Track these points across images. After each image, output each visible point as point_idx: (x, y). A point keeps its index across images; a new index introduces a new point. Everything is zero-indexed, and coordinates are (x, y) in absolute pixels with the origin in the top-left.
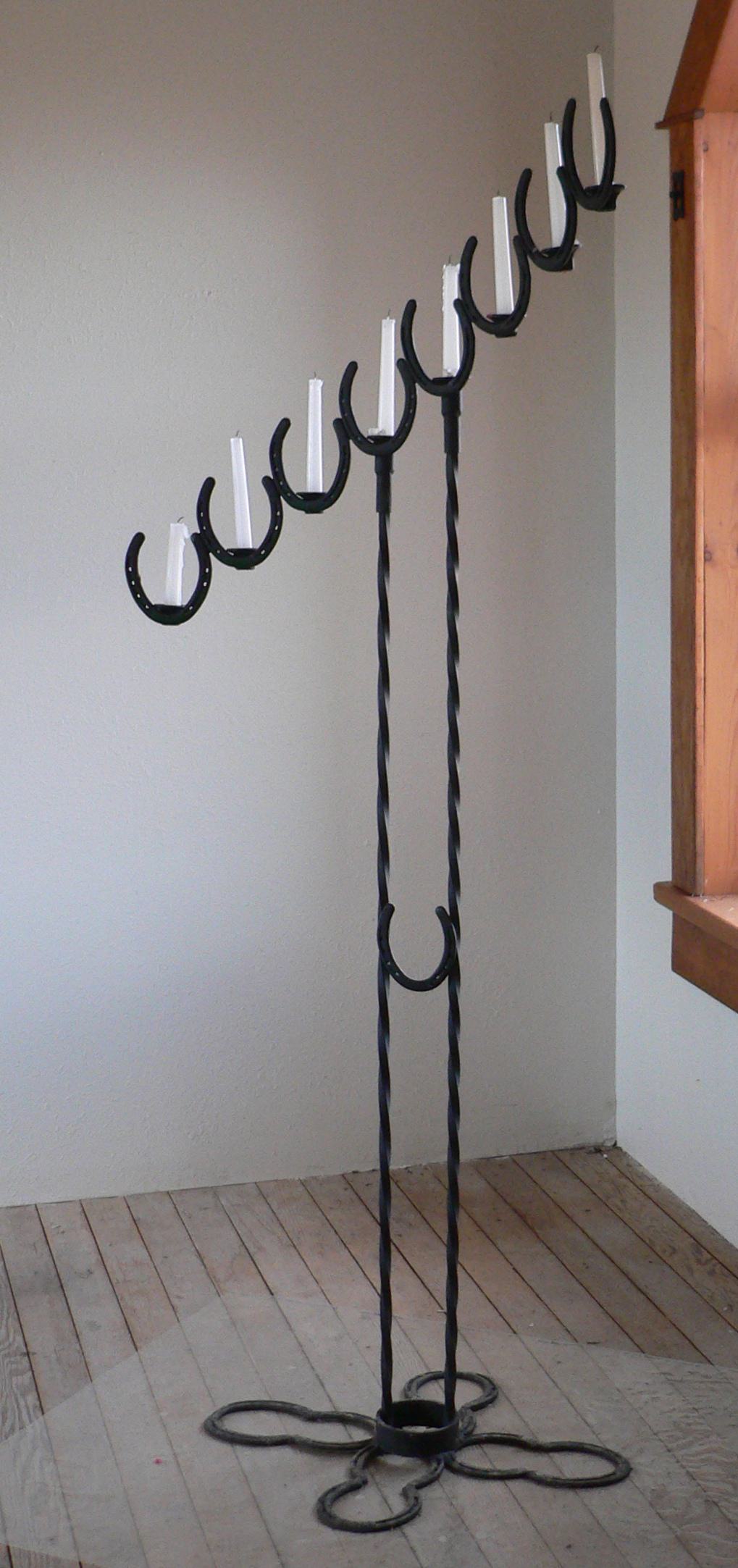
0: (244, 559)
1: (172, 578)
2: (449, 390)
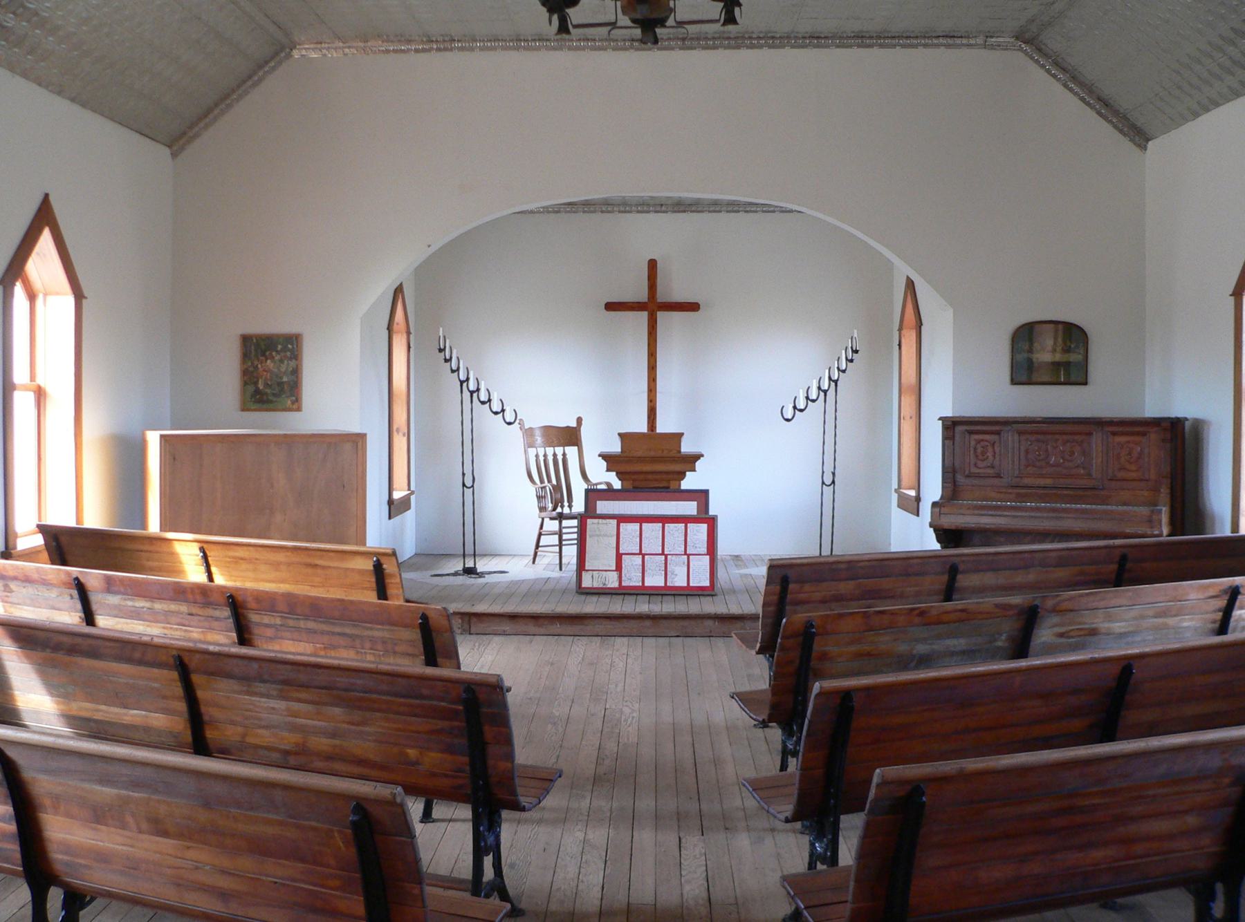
0: (801, 410)
1: (789, 413)
2: (836, 382)
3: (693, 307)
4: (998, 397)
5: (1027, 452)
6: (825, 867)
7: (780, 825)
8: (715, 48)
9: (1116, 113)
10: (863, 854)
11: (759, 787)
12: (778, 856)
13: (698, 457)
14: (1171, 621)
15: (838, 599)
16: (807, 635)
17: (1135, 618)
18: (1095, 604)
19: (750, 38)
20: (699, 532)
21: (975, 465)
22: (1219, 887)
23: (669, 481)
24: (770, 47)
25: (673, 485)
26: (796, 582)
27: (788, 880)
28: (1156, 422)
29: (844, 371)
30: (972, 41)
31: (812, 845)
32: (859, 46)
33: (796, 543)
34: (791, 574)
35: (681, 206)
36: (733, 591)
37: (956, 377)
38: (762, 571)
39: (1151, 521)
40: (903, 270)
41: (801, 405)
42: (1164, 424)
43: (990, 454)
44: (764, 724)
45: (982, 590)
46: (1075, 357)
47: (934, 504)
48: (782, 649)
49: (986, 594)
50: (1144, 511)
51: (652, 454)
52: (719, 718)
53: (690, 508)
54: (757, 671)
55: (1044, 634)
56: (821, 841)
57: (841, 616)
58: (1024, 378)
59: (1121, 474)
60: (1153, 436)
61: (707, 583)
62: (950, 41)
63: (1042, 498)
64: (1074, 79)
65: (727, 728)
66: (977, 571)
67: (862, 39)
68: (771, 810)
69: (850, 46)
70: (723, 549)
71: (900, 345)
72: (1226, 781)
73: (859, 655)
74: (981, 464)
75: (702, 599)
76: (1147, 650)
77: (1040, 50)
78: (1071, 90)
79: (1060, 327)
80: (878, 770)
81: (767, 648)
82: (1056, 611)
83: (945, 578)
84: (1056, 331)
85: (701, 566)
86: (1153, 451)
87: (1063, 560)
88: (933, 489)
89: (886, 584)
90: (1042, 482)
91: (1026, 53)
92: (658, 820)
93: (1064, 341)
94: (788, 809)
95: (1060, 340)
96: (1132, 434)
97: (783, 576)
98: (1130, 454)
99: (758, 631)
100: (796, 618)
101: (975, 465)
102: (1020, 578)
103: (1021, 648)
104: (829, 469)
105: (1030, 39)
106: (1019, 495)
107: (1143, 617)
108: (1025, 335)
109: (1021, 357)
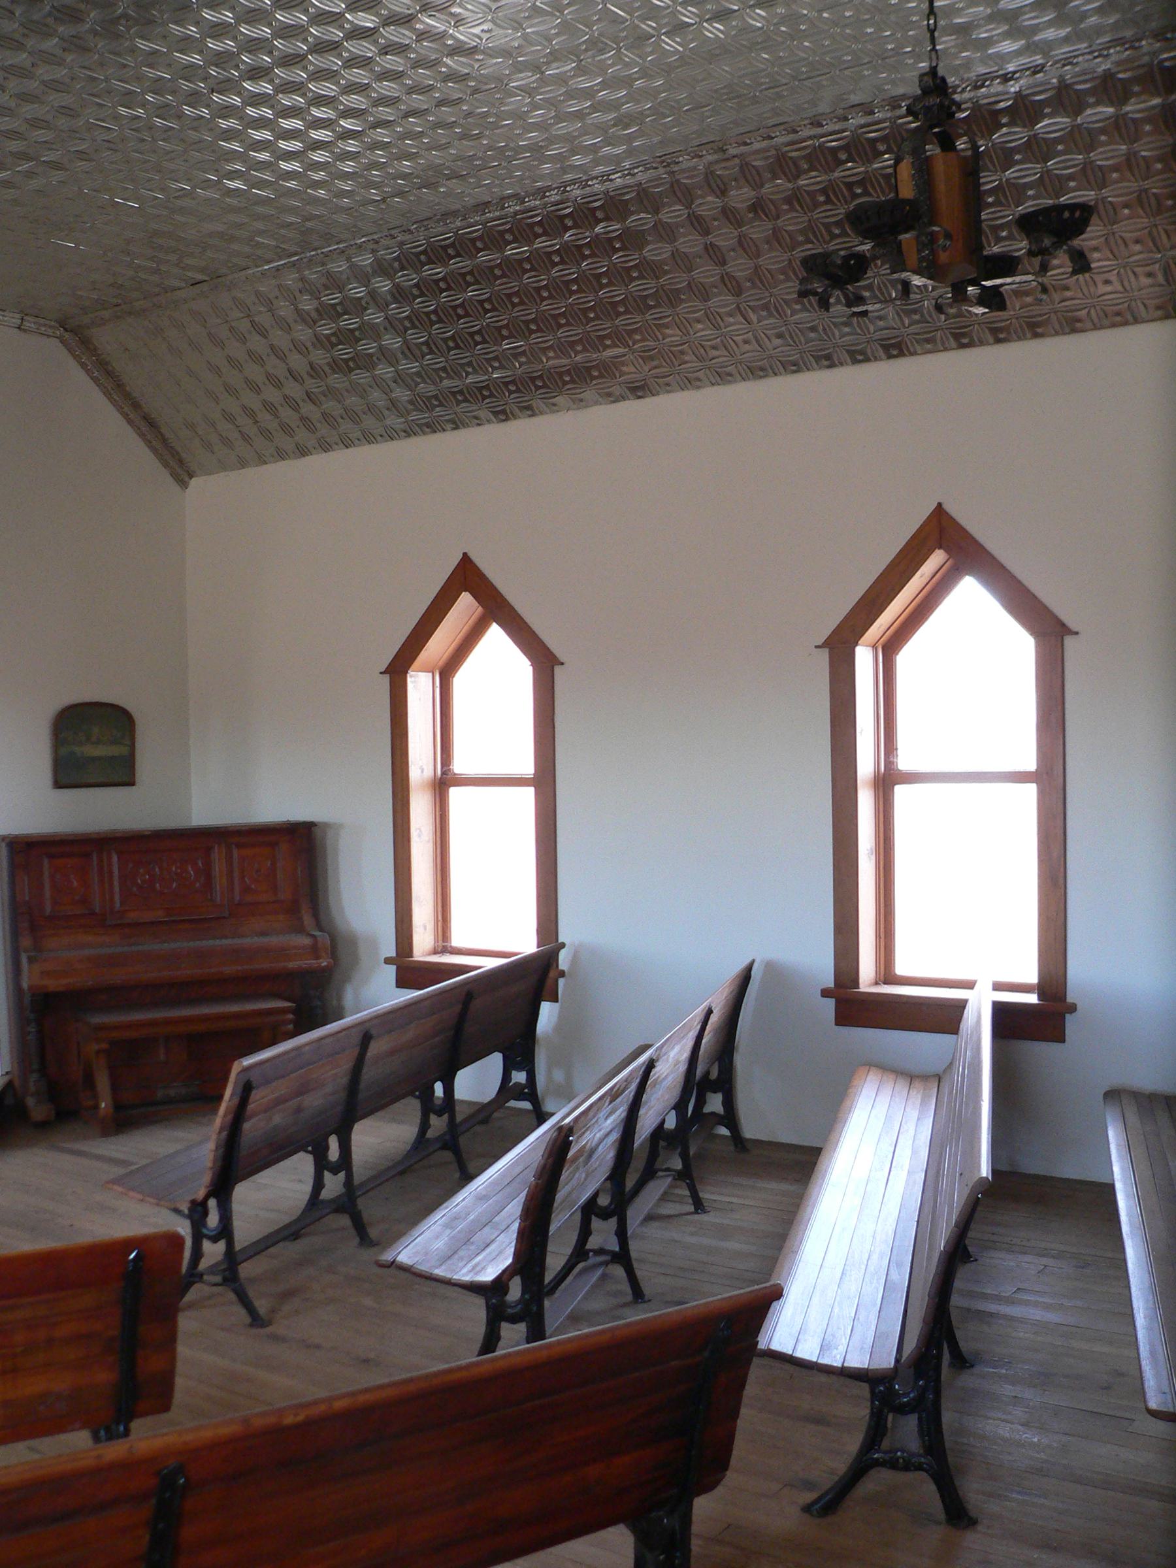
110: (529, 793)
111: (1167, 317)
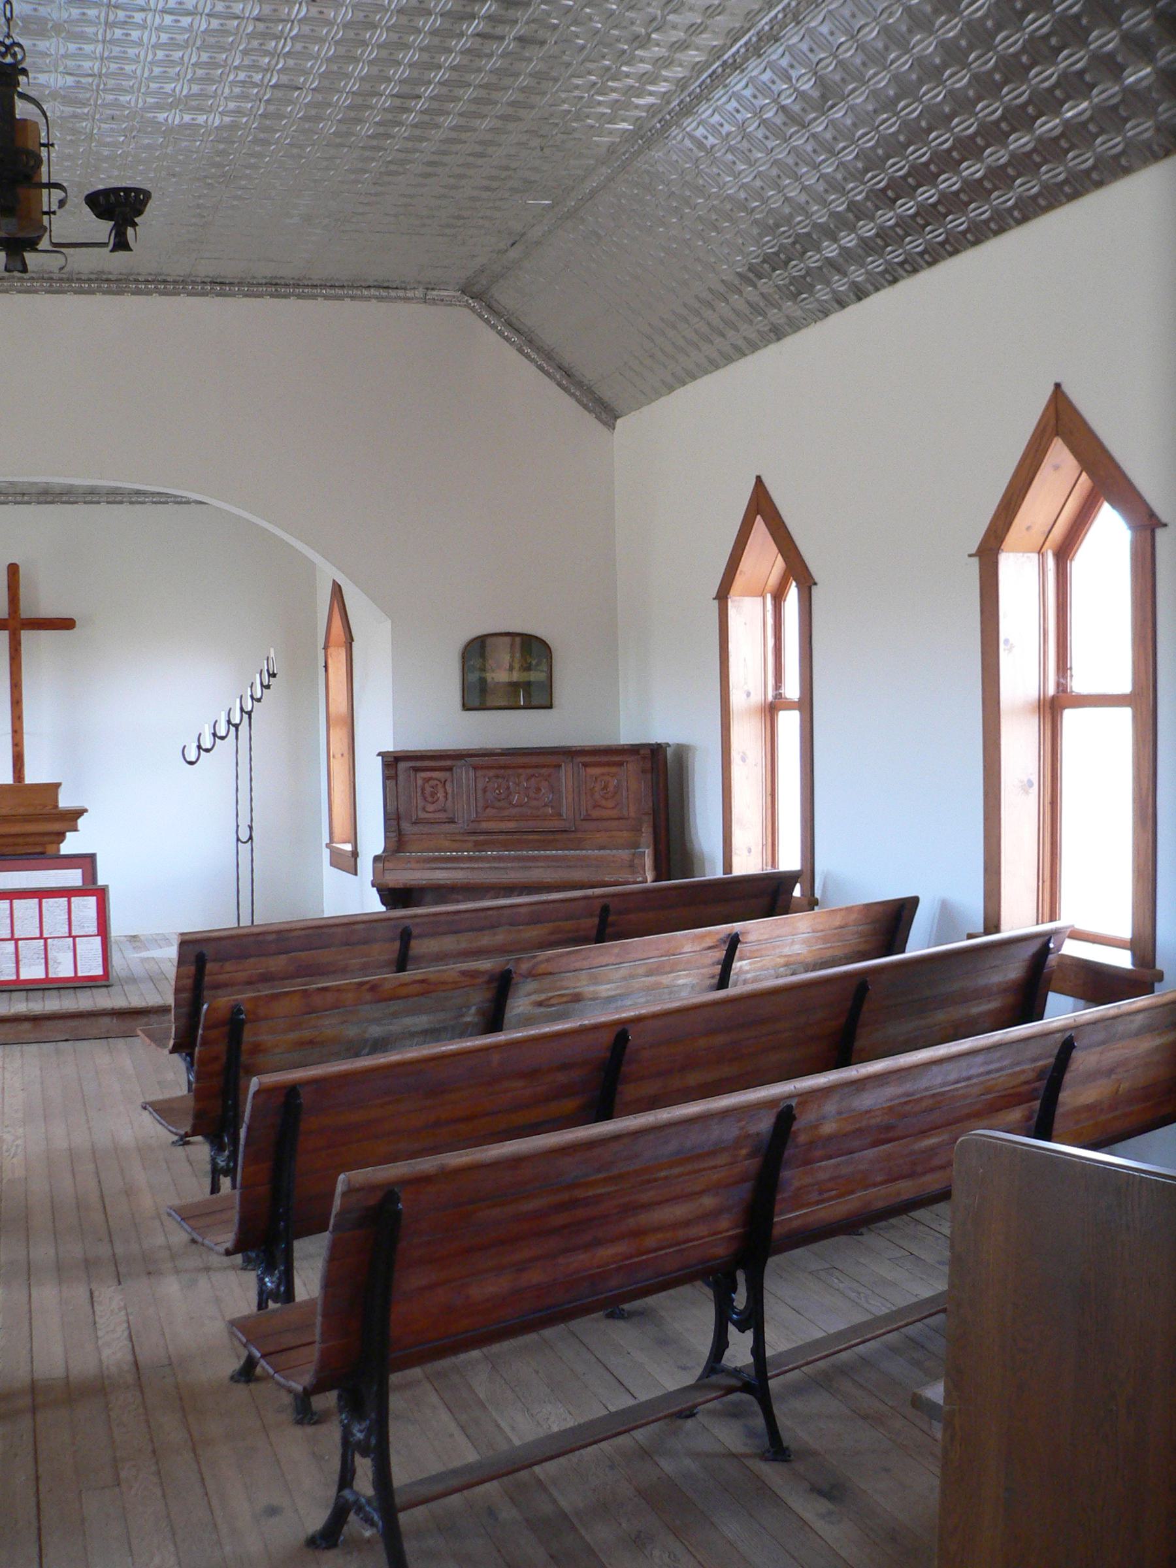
0: (207, 750)
1: (192, 755)
2: (249, 714)
3: (67, 624)
4: (448, 726)
5: (485, 791)
6: (278, 1305)
7: (217, 1260)
8: (91, 292)
9: (579, 384)
10: (330, 1282)
11: (188, 1215)
12: (218, 1300)
13: (80, 812)
14: (666, 979)
15: (266, 978)
16: (235, 1024)
17: (624, 979)
18: (578, 965)
19: (136, 281)
20: (86, 907)
21: (424, 809)
22: (741, 1277)
23: (43, 844)
24: (162, 294)
25: (50, 849)
26: (214, 961)
27: (239, 1325)
28: (634, 750)
29: (259, 700)
30: (410, 294)
31: (261, 1280)
32: (272, 296)
33: (212, 915)
34: (208, 951)
35: (47, 496)
36: (133, 980)
37: (398, 703)
38: (172, 952)
39: (633, 866)
40: (327, 573)
41: (207, 742)
42: (642, 752)
43: (441, 795)
44: (183, 1141)
45: (441, 957)
46: (536, 676)
47: (377, 859)
48: (205, 1042)
49: (445, 960)
50: (625, 854)
51: (22, 811)
52: (126, 1137)
53: (73, 877)
54: (170, 1076)
55: (520, 1004)
56: (271, 1275)
57: (275, 997)
58: (477, 704)
59: (595, 813)
60: (631, 767)
61: (100, 972)
62: (383, 293)
63: (506, 846)
64: (530, 342)
65: (139, 1150)
66: (434, 935)
67: (276, 287)
68: (206, 1242)
69: (261, 296)
70: (116, 929)
71: (326, 667)
72: (744, 1152)
73: (302, 1044)
74: (430, 808)
75: (95, 991)
76: (643, 1011)
77: (489, 307)
78: (527, 356)
79: (518, 639)
80: (342, 1177)
81: (184, 1045)
82: (532, 975)
83: (397, 945)
84: (512, 645)
85: (90, 950)
86: (632, 784)
87: (536, 917)
88: (373, 840)
89: (324, 956)
90: (504, 826)
91: (473, 309)
92: (61, 1271)
93: (523, 656)
94: (228, 1238)
95: (518, 655)
96: (608, 764)
97: (199, 956)
98: (605, 787)
99: (170, 1025)
100: (216, 1004)
101: (424, 809)
102: (486, 940)
103: (494, 1021)
104: (244, 822)
105: (478, 293)
106: (476, 843)
107: (632, 977)
108: (477, 650)
109: (473, 677)
110: (1126, 713)
111: (1167, 154)
